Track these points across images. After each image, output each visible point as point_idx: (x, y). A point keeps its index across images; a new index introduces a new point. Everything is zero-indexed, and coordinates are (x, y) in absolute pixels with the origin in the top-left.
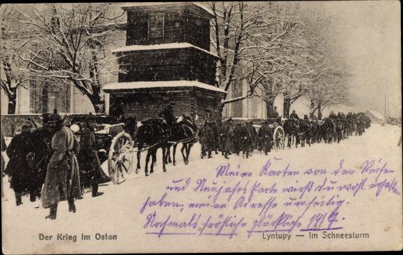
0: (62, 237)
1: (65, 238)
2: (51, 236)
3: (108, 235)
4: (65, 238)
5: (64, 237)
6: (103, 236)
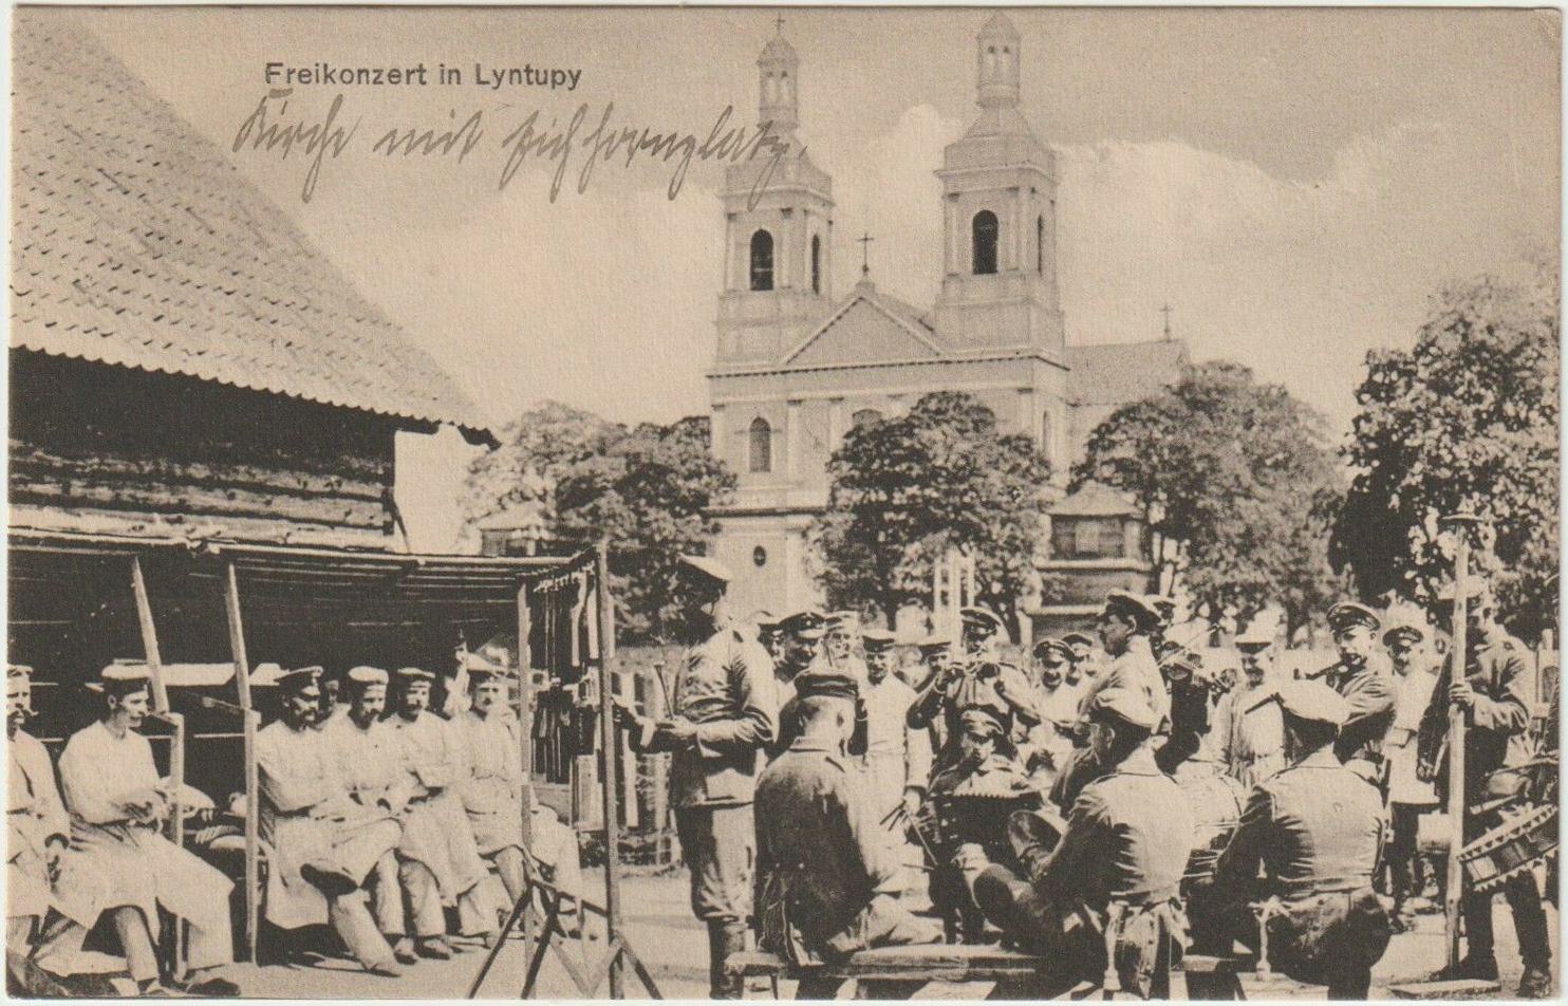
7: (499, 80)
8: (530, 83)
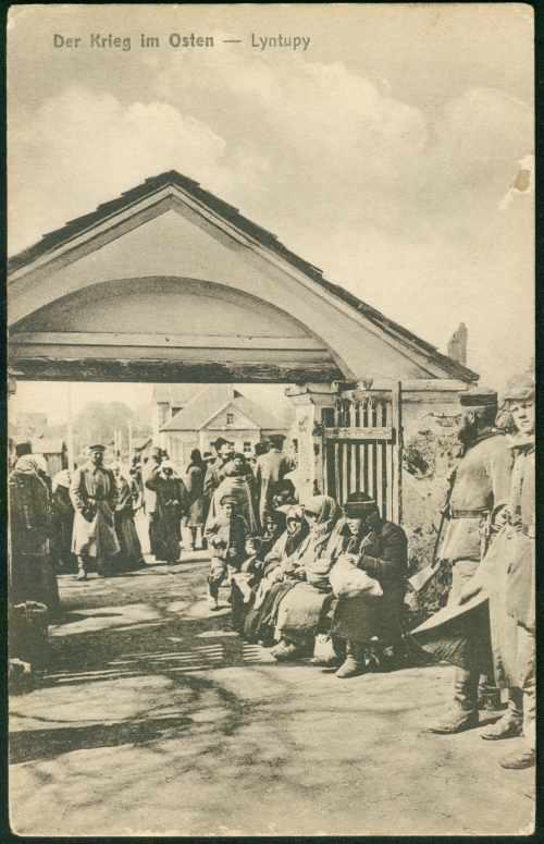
0: (100, 41)
1: (107, 43)
2: (77, 40)
3: (196, 36)
4: (107, 43)
5: (104, 40)
6: (185, 39)
7: (264, 45)
8: (193, 45)
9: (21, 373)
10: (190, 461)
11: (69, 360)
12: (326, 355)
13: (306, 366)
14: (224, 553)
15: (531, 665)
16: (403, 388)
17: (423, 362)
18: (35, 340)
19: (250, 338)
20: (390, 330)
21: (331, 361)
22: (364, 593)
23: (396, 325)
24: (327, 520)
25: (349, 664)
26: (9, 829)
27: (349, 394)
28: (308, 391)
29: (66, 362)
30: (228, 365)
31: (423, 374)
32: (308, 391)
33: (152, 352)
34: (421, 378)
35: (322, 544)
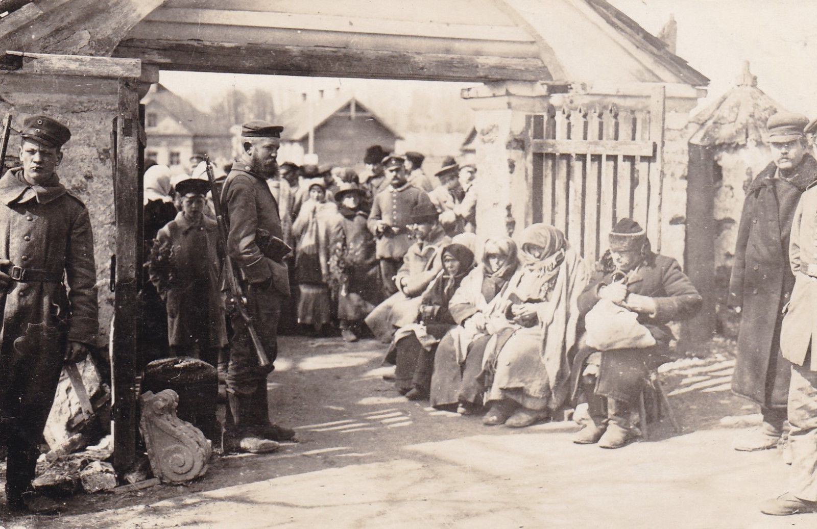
9: (168, 61)
10: (648, 237)
11: (227, 45)
12: (533, 49)
13: (506, 62)
14: (245, 198)
15: (133, 150)
16: (668, 95)
17: (647, 60)
18: (191, 19)
19: (448, 24)
20: (615, 20)
21: (536, 57)
22: (681, 382)
23: (622, 14)
24: (553, 253)
25: (614, 432)
26: (202, 429)
27: (556, 99)
28: (508, 94)
29: (223, 48)
30: (419, 59)
31: (647, 76)
32: (508, 94)
33: (331, 38)
34: (644, 81)
35: (549, 281)
